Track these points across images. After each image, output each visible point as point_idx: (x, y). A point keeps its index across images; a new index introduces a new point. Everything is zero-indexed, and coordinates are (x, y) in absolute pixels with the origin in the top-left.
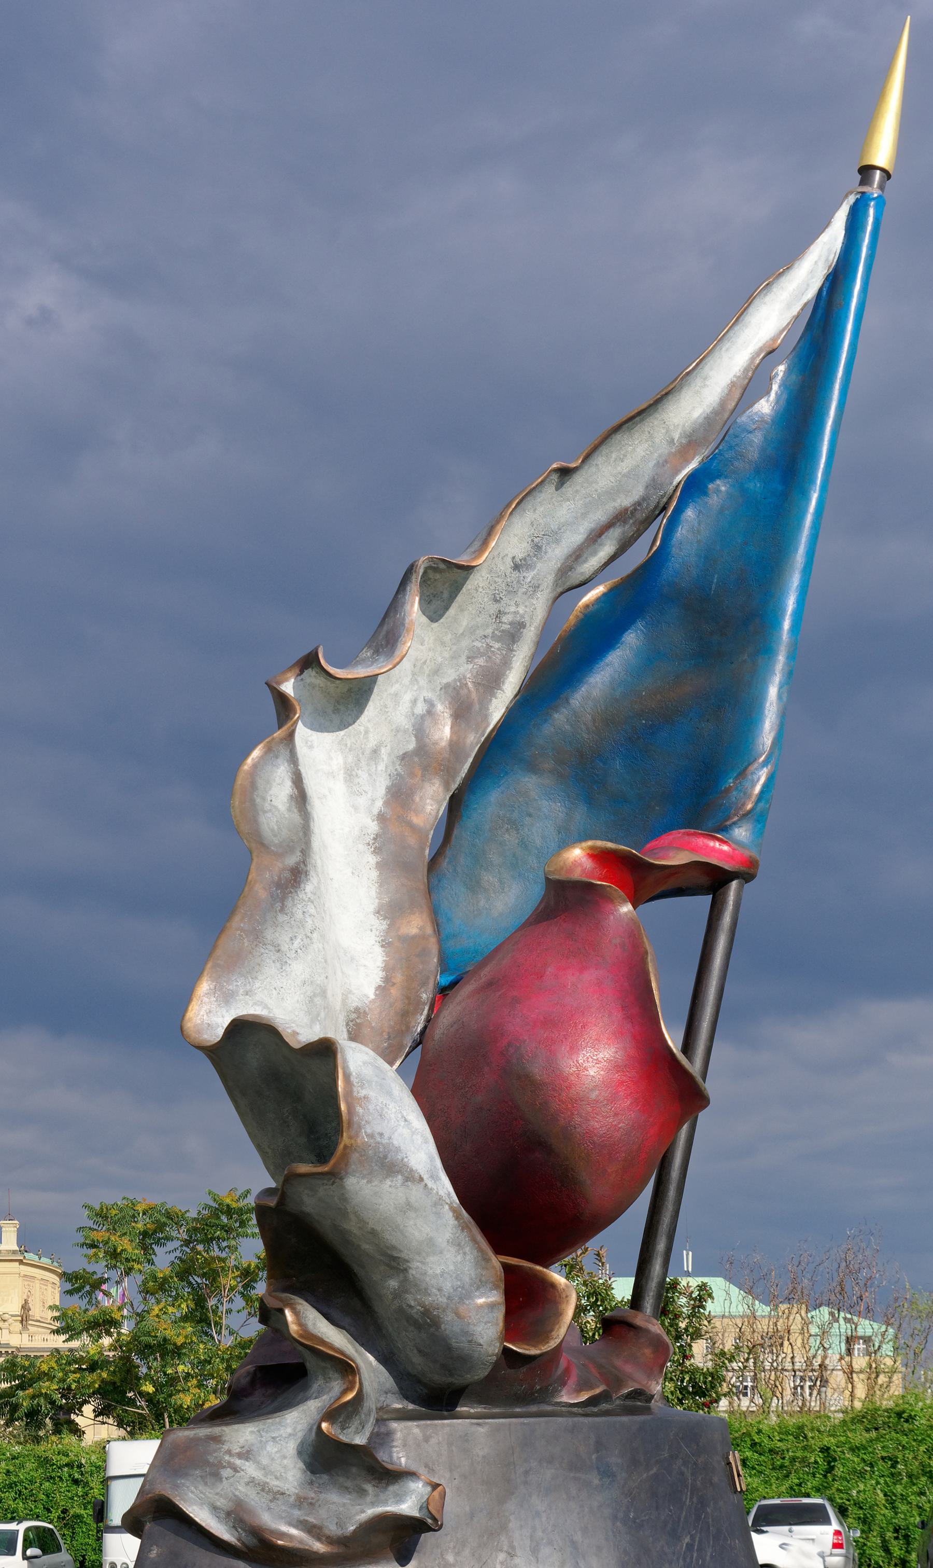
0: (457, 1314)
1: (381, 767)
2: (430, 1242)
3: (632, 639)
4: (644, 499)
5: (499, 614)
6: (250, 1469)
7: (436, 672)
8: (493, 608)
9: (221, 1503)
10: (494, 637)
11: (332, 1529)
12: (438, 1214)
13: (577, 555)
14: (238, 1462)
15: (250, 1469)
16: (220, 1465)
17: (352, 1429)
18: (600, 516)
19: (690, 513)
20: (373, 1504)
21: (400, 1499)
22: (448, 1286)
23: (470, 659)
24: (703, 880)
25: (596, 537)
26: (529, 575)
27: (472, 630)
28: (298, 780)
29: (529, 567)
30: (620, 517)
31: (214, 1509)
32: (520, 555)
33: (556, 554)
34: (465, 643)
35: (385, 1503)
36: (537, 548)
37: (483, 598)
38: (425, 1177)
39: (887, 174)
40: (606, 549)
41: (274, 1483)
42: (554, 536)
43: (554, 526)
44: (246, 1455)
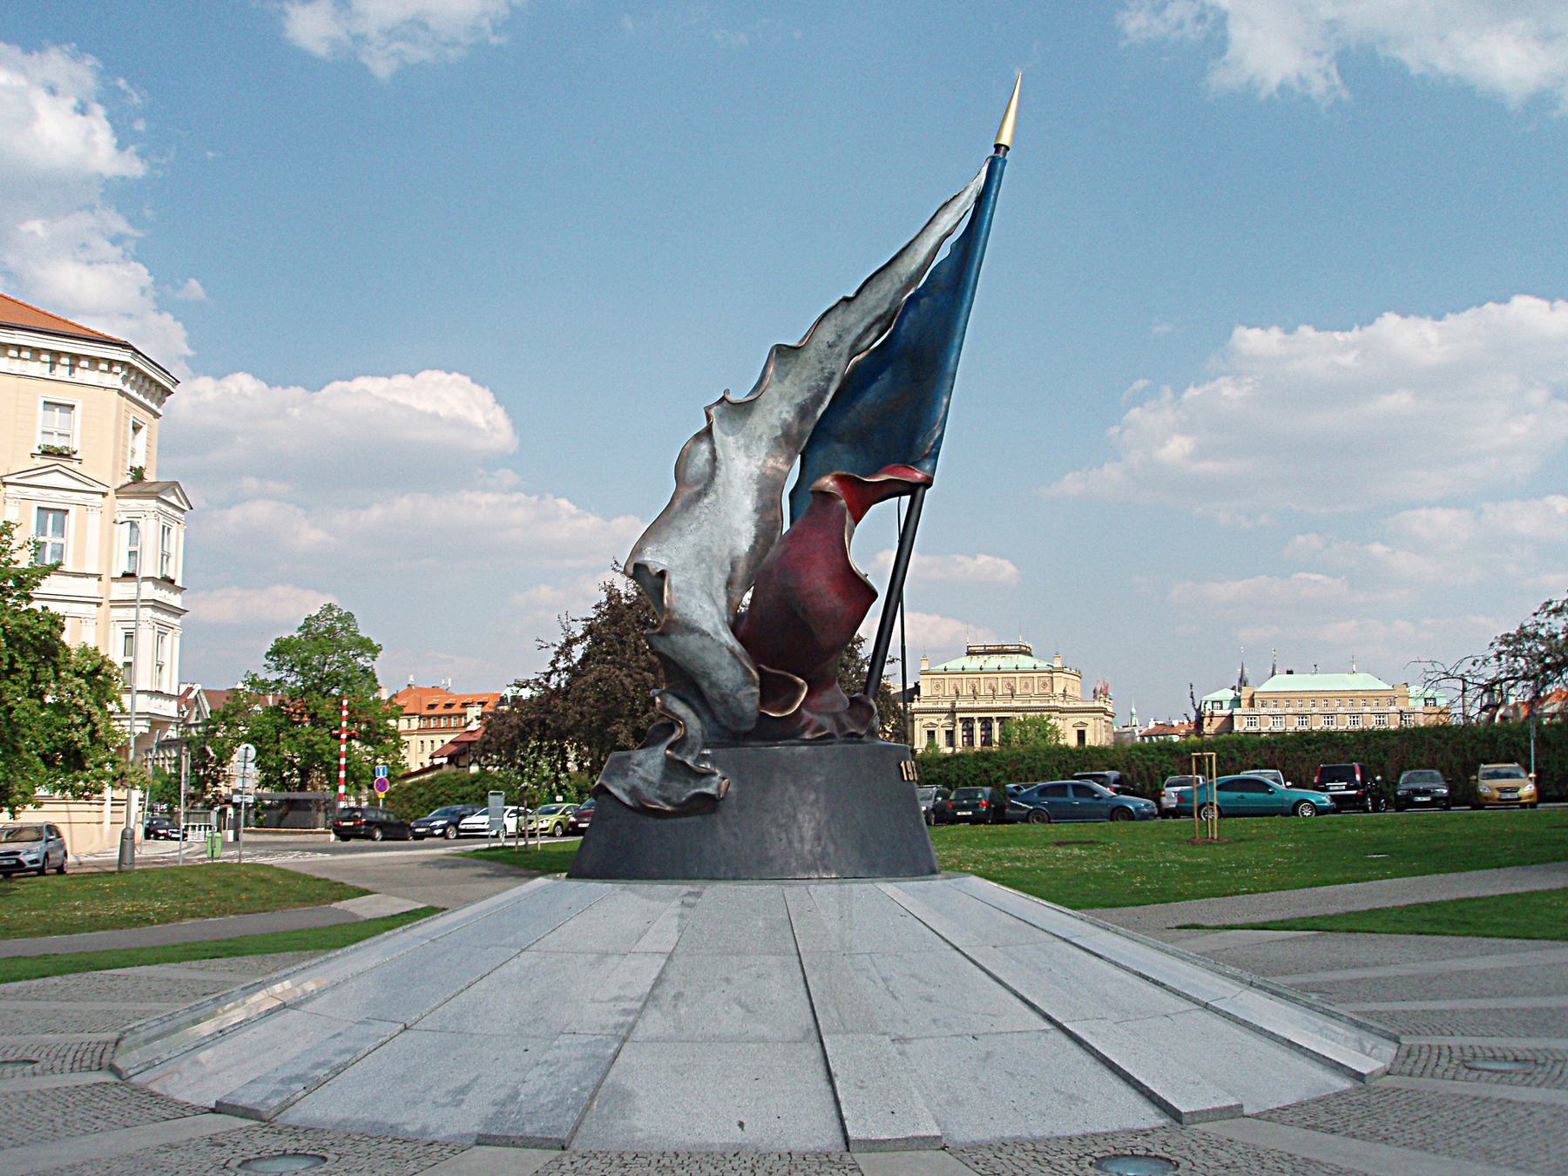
0: (735, 698)
1: (763, 444)
2: (718, 664)
3: (885, 378)
4: (889, 309)
5: (823, 369)
6: (640, 771)
7: (793, 398)
8: (820, 366)
9: (627, 787)
10: (821, 380)
11: (675, 799)
12: (721, 651)
13: (860, 338)
14: (636, 768)
15: (640, 771)
16: (629, 769)
17: (684, 753)
18: (869, 319)
19: (911, 314)
20: (694, 788)
21: (707, 785)
22: (730, 685)
23: (809, 390)
24: (908, 488)
25: (868, 330)
26: (837, 350)
27: (810, 378)
28: (713, 452)
29: (836, 346)
30: (879, 319)
31: (624, 790)
32: (831, 341)
33: (849, 339)
34: (806, 384)
35: (701, 787)
36: (840, 336)
37: (814, 361)
38: (712, 634)
39: (1007, 148)
40: (873, 335)
41: (650, 778)
42: (848, 330)
43: (848, 326)
44: (639, 765)
